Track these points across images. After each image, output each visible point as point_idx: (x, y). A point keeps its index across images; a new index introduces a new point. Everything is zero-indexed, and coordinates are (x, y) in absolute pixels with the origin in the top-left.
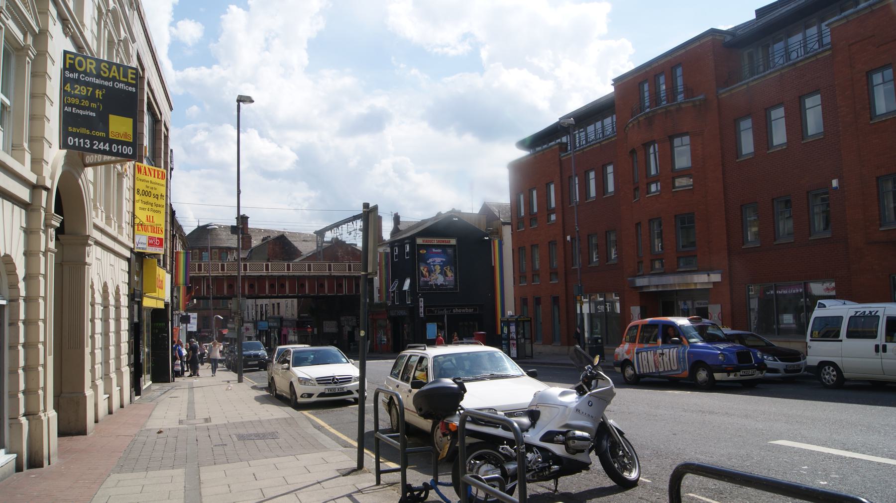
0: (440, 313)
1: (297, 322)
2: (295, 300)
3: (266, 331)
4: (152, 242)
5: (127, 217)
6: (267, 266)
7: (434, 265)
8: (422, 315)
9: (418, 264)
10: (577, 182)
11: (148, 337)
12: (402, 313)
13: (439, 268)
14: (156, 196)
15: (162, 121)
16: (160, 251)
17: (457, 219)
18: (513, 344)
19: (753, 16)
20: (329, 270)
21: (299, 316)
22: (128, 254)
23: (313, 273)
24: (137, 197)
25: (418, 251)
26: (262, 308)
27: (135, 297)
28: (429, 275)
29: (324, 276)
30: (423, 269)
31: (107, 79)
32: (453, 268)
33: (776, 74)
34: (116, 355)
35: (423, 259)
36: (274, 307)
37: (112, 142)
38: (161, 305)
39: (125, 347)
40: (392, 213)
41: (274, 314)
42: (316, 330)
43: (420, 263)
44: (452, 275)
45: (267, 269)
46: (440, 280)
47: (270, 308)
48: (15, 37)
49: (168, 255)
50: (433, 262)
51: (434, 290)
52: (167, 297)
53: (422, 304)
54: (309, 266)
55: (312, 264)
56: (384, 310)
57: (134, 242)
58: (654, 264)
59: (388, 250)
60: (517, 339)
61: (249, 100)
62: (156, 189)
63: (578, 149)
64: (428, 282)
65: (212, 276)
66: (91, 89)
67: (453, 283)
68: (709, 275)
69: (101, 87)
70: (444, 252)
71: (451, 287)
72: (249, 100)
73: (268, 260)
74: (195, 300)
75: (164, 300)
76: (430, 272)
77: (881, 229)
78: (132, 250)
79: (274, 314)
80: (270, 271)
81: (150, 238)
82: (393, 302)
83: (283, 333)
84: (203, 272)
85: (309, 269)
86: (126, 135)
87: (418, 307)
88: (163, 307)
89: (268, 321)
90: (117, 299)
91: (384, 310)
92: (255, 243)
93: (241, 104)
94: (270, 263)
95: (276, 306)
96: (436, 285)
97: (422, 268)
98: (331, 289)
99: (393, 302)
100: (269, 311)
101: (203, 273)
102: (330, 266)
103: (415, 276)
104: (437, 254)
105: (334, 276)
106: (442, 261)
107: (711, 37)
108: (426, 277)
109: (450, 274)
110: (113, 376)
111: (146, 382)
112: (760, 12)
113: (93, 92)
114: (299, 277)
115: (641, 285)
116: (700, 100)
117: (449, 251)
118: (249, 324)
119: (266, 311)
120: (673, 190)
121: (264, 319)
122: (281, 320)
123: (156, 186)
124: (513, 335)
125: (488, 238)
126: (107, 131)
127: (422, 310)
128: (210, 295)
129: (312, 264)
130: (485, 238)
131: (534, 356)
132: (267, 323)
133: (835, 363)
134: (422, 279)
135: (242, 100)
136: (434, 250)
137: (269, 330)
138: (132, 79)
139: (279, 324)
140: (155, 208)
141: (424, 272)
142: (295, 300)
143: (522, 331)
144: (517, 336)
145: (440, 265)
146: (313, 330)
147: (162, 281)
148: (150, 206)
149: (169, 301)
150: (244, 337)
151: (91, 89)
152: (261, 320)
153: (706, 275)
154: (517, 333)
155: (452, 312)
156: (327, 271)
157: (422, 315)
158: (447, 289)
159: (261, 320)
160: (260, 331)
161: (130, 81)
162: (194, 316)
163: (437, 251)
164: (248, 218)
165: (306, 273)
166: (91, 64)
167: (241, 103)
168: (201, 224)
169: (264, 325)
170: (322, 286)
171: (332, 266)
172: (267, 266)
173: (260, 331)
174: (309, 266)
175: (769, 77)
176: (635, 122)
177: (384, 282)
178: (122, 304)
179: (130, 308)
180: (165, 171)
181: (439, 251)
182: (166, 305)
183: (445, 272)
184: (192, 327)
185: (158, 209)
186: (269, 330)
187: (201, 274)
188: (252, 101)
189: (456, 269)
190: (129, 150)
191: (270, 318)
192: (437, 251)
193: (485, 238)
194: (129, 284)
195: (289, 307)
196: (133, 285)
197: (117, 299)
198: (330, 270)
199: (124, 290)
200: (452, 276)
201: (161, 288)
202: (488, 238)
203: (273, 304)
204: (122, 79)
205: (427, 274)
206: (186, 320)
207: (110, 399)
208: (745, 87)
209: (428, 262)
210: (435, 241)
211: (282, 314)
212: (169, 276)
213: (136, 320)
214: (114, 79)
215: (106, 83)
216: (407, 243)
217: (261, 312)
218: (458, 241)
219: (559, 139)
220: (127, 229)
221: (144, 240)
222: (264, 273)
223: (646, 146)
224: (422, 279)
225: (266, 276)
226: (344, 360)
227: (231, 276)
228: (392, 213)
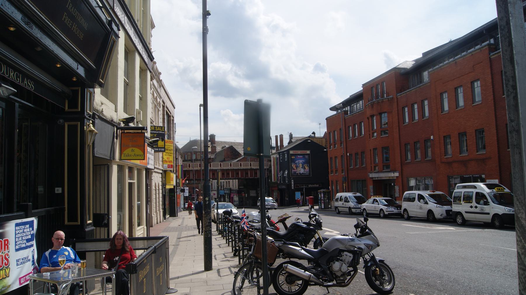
0: (302, 187)
2: (237, 180)
4: (169, 166)
5: (161, 159)
6: (221, 164)
7: (299, 164)
8: (293, 188)
9: (291, 163)
10: (351, 129)
11: (168, 199)
12: (284, 187)
13: (301, 165)
14: (170, 150)
15: (171, 116)
16: (172, 169)
17: (310, 141)
18: (323, 202)
19: (421, 56)
20: (250, 166)
22: (161, 172)
23: (242, 167)
25: (291, 157)
26: (221, 184)
27: (164, 185)
28: (297, 169)
29: (248, 169)
30: (293, 166)
31: (157, 131)
32: (308, 165)
33: (414, 90)
34: (155, 207)
35: (293, 161)
36: (227, 183)
37: (159, 148)
38: (172, 187)
39: (161, 203)
40: (288, 132)
41: (227, 186)
42: (246, 195)
43: (292, 163)
44: (308, 168)
45: (221, 166)
46: (302, 171)
47: (225, 184)
49: (175, 170)
50: (298, 162)
51: (299, 176)
52: (175, 184)
53: (293, 183)
54: (241, 164)
55: (242, 163)
56: (276, 185)
57: (163, 167)
58: (376, 168)
59: (278, 156)
60: (324, 200)
62: (170, 148)
63: (354, 113)
64: (296, 172)
65: (195, 170)
66: (153, 134)
67: (308, 172)
68: (394, 173)
69: (155, 133)
70: (304, 157)
71: (308, 174)
73: (222, 161)
74: (187, 181)
75: (173, 185)
76: (297, 167)
77: (445, 157)
78: (162, 170)
79: (227, 186)
80: (222, 167)
81: (168, 165)
82: (280, 181)
83: (232, 196)
84: (191, 168)
85: (241, 166)
86: (162, 145)
87: (291, 184)
88: (173, 188)
89: (224, 190)
90: (159, 187)
91: (276, 185)
92: (219, 149)
94: (222, 163)
95: (228, 182)
96: (300, 173)
97: (293, 165)
98: (251, 175)
99: (280, 181)
100: (224, 185)
101: (191, 169)
103: (289, 168)
104: (300, 159)
106: (303, 162)
107: (394, 71)
108: (295, 169)
109: (307, 168)
110: (158, 212)
111: (168, 216)
112: (425, 54)
113: (154, 135)
114: (236, 170)
116: (390, 98)
117: (306, 157)
118: (215, 192)
119: (223, 185)
120: (381, 136)
121: (222, 189)
123: (170, 146)
124: (322, 198)
125: (326, 150)
126: (158, 145)
127: (293, 186)
128: (194, 178)
129: (242, 163)
130: (325, 150)
131: (332, 208)
133: (432, 211)
134: (293, 171)
136: (299, 156)
137: (225, 195)
138: (163, 130)
139: (229, 192)
140: (170, 154)
141: (294, 167)
142: (237, 180)
143: (327, 197)
144: (324, 199)
145: (302, 164)
146: (245, 195)
147: (172, 178)
148: (168, 154)
149: (175, 185)
150: (213, 198)
151: (153, 134)
152: (221, 189)
153: (393, 173)
154: (324, 197)
155: (308, 186)
157: (293, 188)
158: (305, 175)
159: (221, 189)
161: (163, 130)
162: (187, 189)
163: (300, 157)
165: (239, 167)
166: (153, 127)
168: (191, 140)
169: (222, 192)
170: (247, 174)
172: (221, 164)
174: (241, 164)
175: (412, 91)
176: (370, 105)
177: (276, 172)
178: (160, 189)
179: (162, 189)
180: (173, 141)
181: (301, 157)
182: (174, 187)
183: (304, 167)
184: (186, 194)
185: (171, 154)
186: (225, 195)
187: (190, 169)
189: (310, 165)
190: (163, 150)
191: (225, 189)
192: (300, 157)
193: (325, 150)
194: (162, 182)
195: (234, 184)
196: (163, 182)
197: (159, 187)
198: (251, 166)
199: (160, 184)
200: (308, 169)
201: (172, 180)
202: (326, 150)
203: (227, 182)
204: (161, 130)
205: (295, 168)
206: (183, 191)
207: (157, 219)
208: (405, 94)
209: (296, 162)
210: (299, 152)
211: (231, 187)
212: (175, 175)
213: (164, 194)
214: (159, 131)
215: (157, 132)
216: (285, 153)
217: (221, 186)
218: (311, 152)
219: (344, 108)
220: (161, 163)
221: (166, 166)
223: (372, 116)
224: (293, 171)
226: (233, 207)
228: (288, 132)
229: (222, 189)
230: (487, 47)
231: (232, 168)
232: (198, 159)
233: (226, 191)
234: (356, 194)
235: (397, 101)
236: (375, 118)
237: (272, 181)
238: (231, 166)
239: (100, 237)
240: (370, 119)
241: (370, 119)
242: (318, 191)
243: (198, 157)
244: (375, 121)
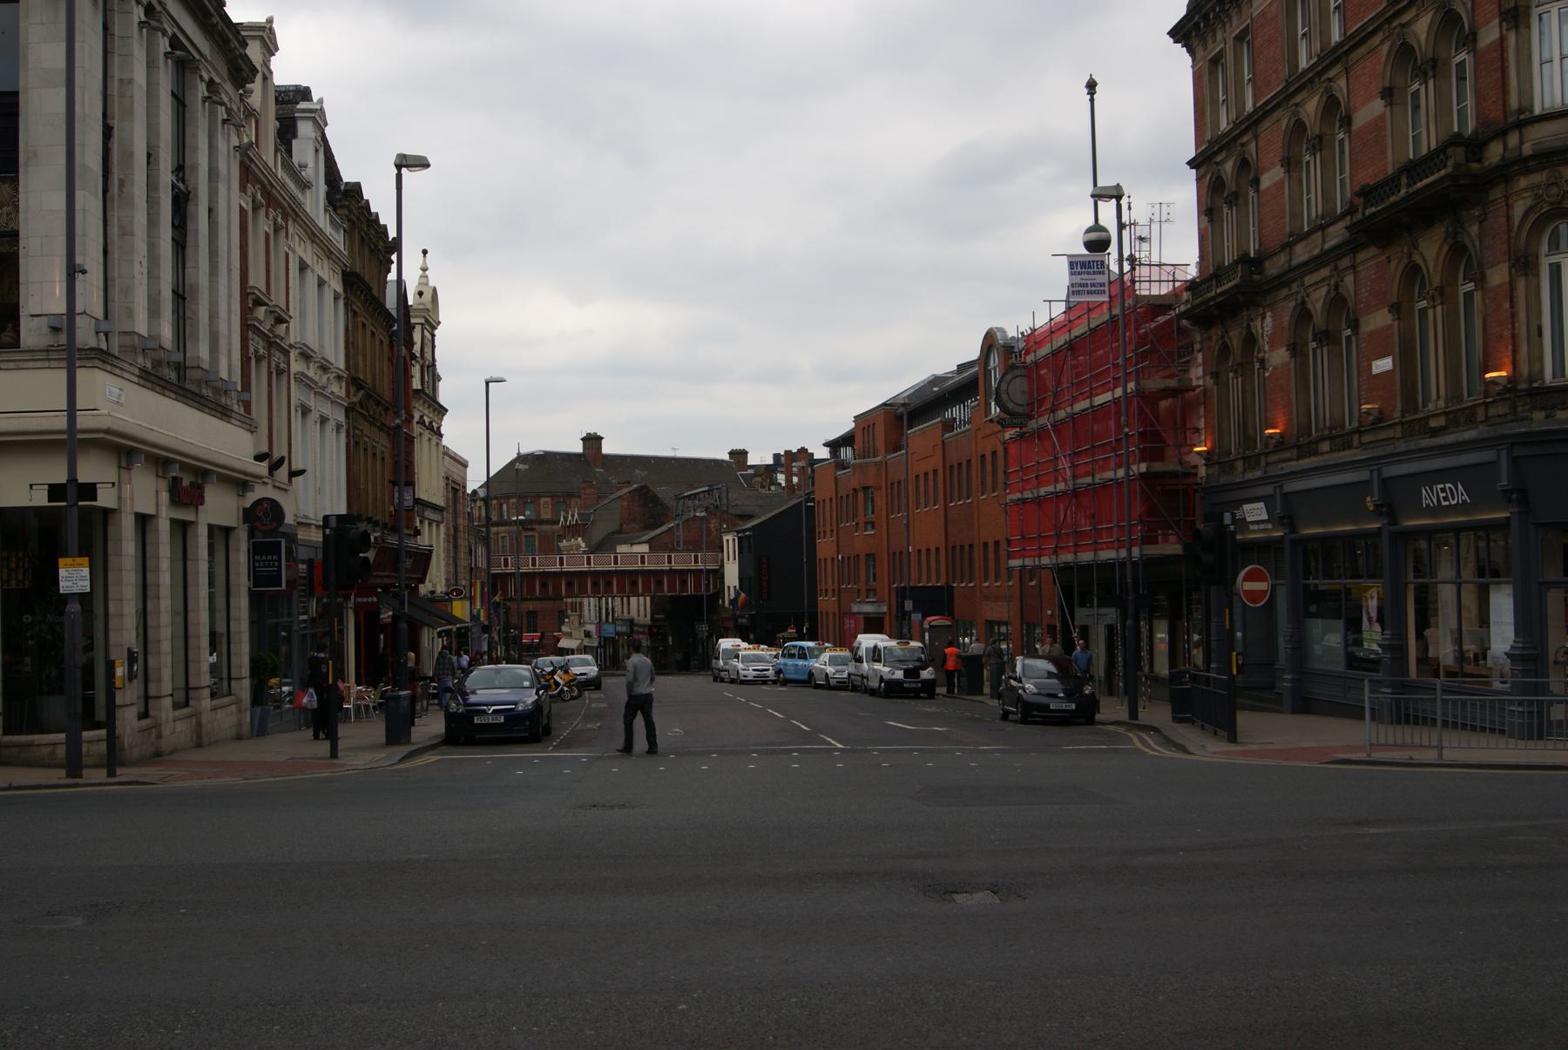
1: (650, 627)
3: (614, 638)
21: (652, 619)
45: (589, 563)
48: (740, 553)
61: (422, 163)
72: (422, 163)
93: (404, 170)
94: (592, 556)
100: (616, 609)
102: (669, 557)
115: (1013, 565)
119: (613, 609)
121: (610, 620)
122: (631, 622)
132: (613, 626)
135: (405, 162)
139: (629, 629)
156: (666, 564)
164: (602, 438)
167: (404, 170)
168: (524, 451)
171: (537, 559)
188: (426, 165)
211: (634, 613)
217: (607, 609)
222: (585, 568)
229: (610, 620)
230: (940, 424)
231: (620, 567)
232: (542, 517)
233: (621, 625)
234: (733, 643)
235: (886, 466)
237: (1246, 503)
238: (616, 563)
242: (778, 635)
243: (542, 512)
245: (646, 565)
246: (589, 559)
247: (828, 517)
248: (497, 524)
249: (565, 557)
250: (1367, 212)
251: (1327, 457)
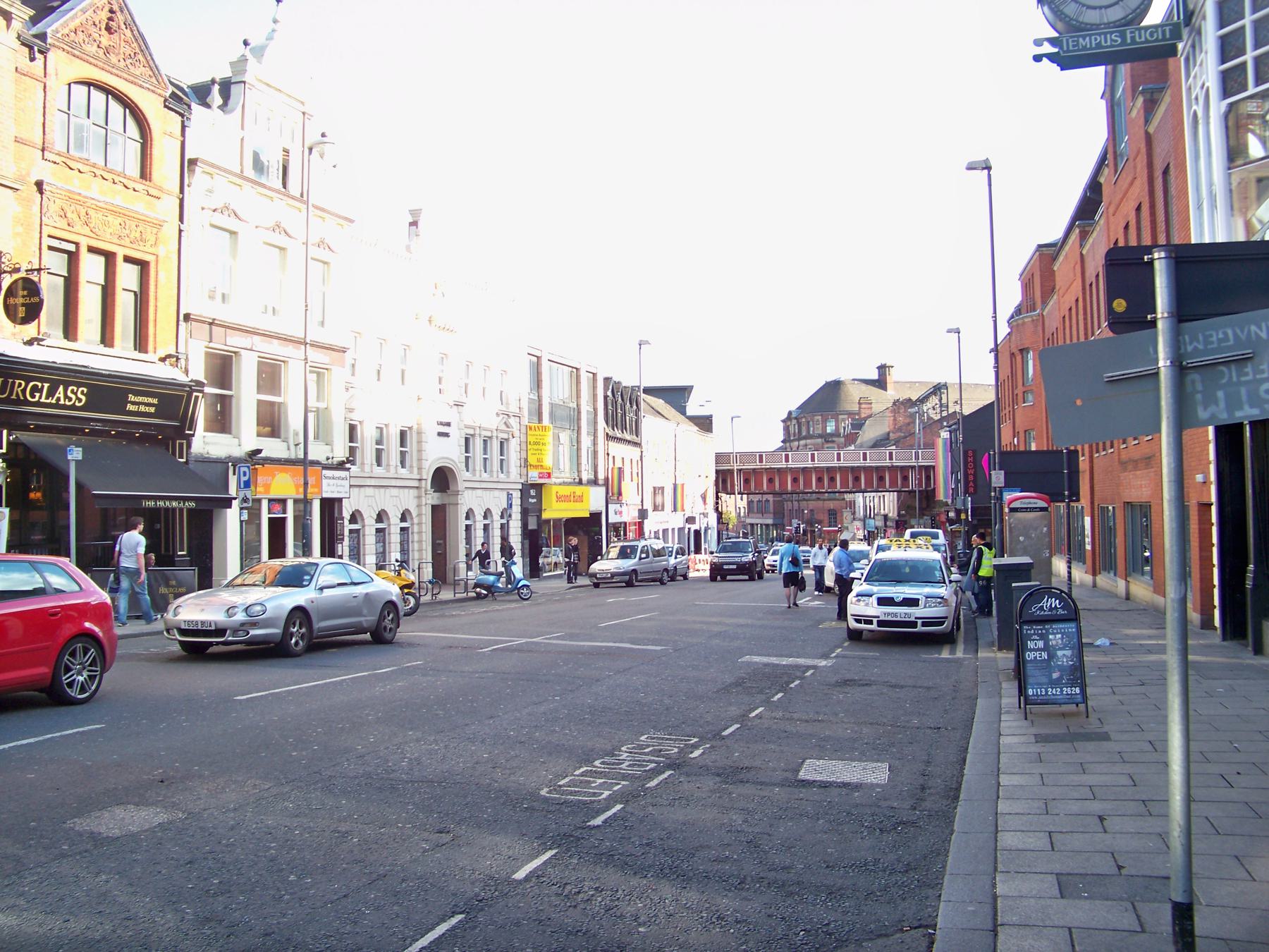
1: (897, 522)
6: (813, 456)
21: (899, 515)
23: (869, 463)
24: (529, 447)
61: (647, 343)
72: (647, 343)
81: (540, 473)
85: (865, 459)
94: (816, 452)
105: (897, 467)
122: (886, 517)
142: (895, 493)
156: (888, 461)
160: (869, 532)
165: (861, 463)
172: (813, 456)
173: (869, 532)
191: (877, 515)
198: (891, 458)
222: (809, 464)
225: (811, 468)
227: (771, 468)
236: (1031, 355)
239: (306, 453)
240: (1019, 358)
241: (1019, 358)
244: (1031, 363)
245: (868, 461)
246: (787, 456)
247: (1007, 393)
248: (805, 438)
249: (790, 453)
250: (230, 638)
251: (1169, 601)
